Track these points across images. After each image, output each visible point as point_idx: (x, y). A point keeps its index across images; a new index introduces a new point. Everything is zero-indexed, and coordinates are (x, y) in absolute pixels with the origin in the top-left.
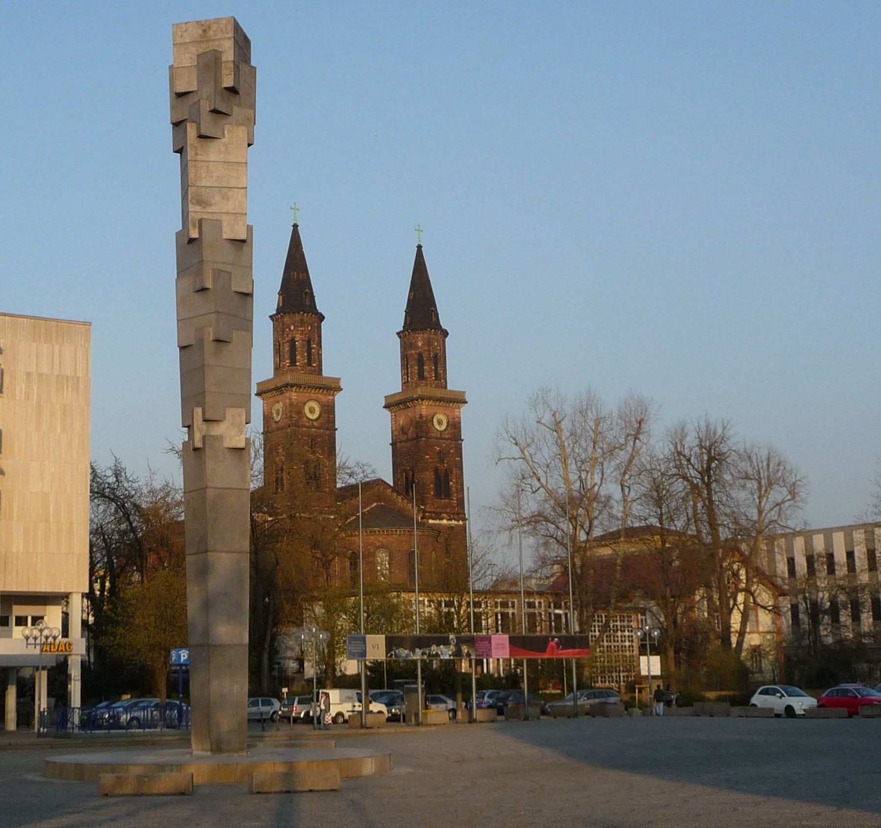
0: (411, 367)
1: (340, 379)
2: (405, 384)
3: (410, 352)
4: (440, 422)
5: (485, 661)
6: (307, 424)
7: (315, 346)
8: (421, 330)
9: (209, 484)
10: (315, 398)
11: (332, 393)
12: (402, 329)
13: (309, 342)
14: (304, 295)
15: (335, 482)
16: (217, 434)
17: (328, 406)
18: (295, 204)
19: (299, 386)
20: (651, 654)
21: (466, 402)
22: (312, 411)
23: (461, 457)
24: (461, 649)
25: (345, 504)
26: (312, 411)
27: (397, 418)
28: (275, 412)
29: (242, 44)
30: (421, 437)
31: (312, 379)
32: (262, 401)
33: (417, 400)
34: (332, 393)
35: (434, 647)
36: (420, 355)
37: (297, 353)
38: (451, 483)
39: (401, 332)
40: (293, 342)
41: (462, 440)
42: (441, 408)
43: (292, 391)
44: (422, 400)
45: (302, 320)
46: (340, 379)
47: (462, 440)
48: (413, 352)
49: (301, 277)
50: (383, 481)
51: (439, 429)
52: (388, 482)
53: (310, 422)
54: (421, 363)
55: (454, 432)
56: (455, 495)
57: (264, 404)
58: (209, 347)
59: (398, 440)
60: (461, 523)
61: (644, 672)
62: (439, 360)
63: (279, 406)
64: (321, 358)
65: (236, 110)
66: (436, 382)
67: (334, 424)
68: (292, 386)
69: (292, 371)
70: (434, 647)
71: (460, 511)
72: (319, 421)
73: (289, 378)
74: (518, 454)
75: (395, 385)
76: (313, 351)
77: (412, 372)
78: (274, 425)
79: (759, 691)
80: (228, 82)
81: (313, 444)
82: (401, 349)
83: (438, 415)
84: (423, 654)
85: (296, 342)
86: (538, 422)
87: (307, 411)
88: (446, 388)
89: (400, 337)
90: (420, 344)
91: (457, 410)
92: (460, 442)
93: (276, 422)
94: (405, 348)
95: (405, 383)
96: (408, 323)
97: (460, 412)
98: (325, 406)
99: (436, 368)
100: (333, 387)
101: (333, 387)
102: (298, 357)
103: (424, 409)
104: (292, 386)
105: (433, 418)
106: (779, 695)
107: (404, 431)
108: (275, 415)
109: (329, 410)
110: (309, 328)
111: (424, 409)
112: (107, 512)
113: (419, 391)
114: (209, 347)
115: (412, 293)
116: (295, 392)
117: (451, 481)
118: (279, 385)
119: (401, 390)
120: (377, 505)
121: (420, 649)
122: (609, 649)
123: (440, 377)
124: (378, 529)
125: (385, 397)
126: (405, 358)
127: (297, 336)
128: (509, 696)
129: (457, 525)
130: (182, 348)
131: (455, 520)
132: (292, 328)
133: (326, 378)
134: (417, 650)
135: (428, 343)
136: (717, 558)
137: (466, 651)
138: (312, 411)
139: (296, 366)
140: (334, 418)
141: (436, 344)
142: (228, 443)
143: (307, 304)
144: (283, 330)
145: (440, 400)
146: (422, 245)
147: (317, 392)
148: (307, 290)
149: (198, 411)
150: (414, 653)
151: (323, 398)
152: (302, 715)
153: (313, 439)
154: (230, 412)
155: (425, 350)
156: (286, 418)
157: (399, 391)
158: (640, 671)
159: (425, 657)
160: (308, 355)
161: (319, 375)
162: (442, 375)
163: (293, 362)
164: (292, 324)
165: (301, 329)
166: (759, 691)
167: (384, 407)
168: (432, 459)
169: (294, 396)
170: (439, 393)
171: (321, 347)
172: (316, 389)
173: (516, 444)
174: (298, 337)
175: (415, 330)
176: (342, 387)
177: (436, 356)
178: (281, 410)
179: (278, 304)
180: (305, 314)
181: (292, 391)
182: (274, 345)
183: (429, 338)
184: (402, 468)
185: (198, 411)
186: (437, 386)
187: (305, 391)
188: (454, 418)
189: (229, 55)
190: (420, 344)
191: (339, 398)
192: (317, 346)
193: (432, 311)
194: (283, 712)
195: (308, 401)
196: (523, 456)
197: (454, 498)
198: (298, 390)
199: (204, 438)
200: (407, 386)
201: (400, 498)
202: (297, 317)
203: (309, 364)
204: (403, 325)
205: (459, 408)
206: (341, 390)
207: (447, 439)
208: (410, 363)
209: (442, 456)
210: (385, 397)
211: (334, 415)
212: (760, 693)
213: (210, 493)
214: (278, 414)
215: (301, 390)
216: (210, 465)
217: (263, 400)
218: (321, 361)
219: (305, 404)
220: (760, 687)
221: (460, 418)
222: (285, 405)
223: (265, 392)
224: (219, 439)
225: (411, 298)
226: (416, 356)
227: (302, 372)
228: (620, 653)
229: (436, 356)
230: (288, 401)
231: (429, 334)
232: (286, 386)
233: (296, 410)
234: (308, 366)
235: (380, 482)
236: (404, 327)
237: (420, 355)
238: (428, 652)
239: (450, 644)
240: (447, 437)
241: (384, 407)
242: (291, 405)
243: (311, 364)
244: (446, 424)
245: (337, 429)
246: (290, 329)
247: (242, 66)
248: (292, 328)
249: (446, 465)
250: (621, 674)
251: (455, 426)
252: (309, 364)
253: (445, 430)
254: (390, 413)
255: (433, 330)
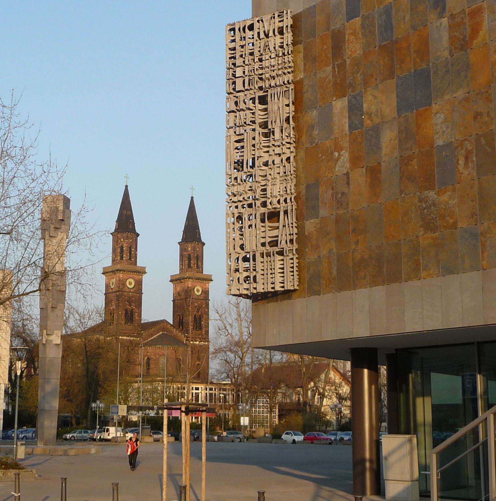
0: (185, 261)
1: (146, 267)
2: (181, 269)
3: (184, 253)
4: (198, 291)
5: (200, 418)
6: (127, 290)
7: (133, 250)
8: (190, 242)
9: (47, 356)
10: (132, 277)
11: (141, 274)
12: (181, 241)
13: (130, 248)
14: (129, 223)
15: (141, 321)
16: (51, 339)
17: (139, 281)
18: (127, 174)
19: (124, 271)
20: (245, 416)
21: (212, 281)
22: (130, 284)
23: (208, 309)
24: (159, 412)
25: (145, 332)
26: (130, 283)
27: (176, 287)
28: (111, 283)
29: (67, 201)
30: (187, 298)
31: (131, 267)
32: (105, 277)
33: (186, 279)
34: (141, 274)
35: (147, 411)
36: (189, 255)
37: (124, 253)
38: (202, 323)
39: (180, 242)
40: (122, 248)
41: (209, 300)
42: (199, 283)
43: (120, 273)
44: (189, 279)
45: (127, 236)
46: (146, 267)
47: (209, 300)
48: (186, 253)
49: (128, 214)
50: (166, 321)
51: (197, 294)
52: (170, 322)
53: (129, 289)
54: (189, 259)
55: (205, 296)
56: (204, 329)
57: (106, 278)
58: (49, 309)
59: (176, 299)
60: (206, 343)
61: (242, 424)
62: (199, 258)
63: (114, 280)
64: (137, 256)
65: (63, 226)
66: (197, 269)
67: (142, 290)
68: (120, 271)
69: (121, 263)
70: (147, 411)
71: (207, 337)
72: (134, 289)
73: (118, 267)
74: (218, 318)
75: (176, 271)
76: (132, 252)
77: (185, 264)
78: (110, 290)
79: (285, 433)
80: (60, 218)
81: (130, 302)
82: (180, 251)
83: (197, 287)
84: (142, 413)
85: (123, 247)
86: (229, 302)
87: (128, 284)
88: (203, 273)
89: (180, 245)
90: (189, 249)
91: (208, 284)
92: (208, 301)
93: (112, 289)
94: (182, 251)
95: (181, 269)
96: (184, 237)
97: (209, 285)
98: (137, 281)
99: (197, 263)
100: (142, 271)
101: (142, 271)
102: (124, 256)
103: (190, 283)
104: (120, 271)
105: (194, 288)
106: (291, 435)
107: (179, 294)
108: (111, 285)
109: (139, 283)
110: (131, 241)
111: (190, 283)
112: (17, 343)
113: (187, 274)
114: (49, 309)
115: (187, 222)
116: (122, 273)
117: (202, 321)
118: (114, 269)
119: (179, 273)
120: (163, 333)
121: (141, 411)
122: (259, 412)
123: (199, 267)
124: (161, 346)
125: (171, 276)
126: (181, 256)
127: (125, 244)
128: (196, 432)
129: (204, 344)
130: (41, 309)
131: (204, 342)
132: (122, 240)
133: (138, 267)
134: (140, 412)
135: (194, 249)
136: (302, 372)
137: (161, 413)
138: (130, 284)
139: (123, 260)
140: (142, 287)
141: (198, 250)
142: (54, 342)
143: (131, 228)
144: (117, 241)
145: (199, 279)
146: (194, 197)
147: (133, 273)
148: (131, 221)
149: (45, 331)
150: (139, 413)
151: (137, 277)
152: (98, 438)
153: (130, 298)
154: (56, 332)
155: (192, 253)
156: (117, 287)
157: (177, 273)
158: (240, 423)
159: (143, 415)
160: (129, 254)
161: (135, 265)
162: (200, 266)
163: (122, 258)
164: (122, 238)
165: (127, 241)
166: (285, 433)
167: (170, 281)
168: (193, 309)
169: (121, 276)
170: (198, 275)
171: (137, 250)
172: (133, 272)
173: (218, 313)
174: (125, 245)
175: (187, 242)
176: (146, 272)
177: (198, 255)
178: (114, 283)
179: (116, 227)
180: (129, 233)
181: (120, 273)
182: (113, 248)
183: (194, 246)
184: (178, 313)
185: (45, 331)
186: (197, 272)
187: (127, 273)
188: (206, 289)
189: (61, 208)
190: (189, 249)
191: (145, 278)
192: (135, 250)
193: (197, 232)
194: (90, 436)
195: (129, 278)
196: (220, 319)
197: (204, 330)
198: (123, 272)
199: (46, 340)
200: (182, 271)
201: (175, 329)
202: (125, 235)
203: (130, 259)
204: (181, 239)
205: (208, 283)
206: (146, 273)
207: (202, 300)
208: (184, 259)
209: (199, 308)
210: (171, 276)
211: (142, 286)
212: (285, 434)
213: (48, 359)
214: (113, 284)
215: (125, 273)
216: (48, 349)
217: (106, 276)
218: (137, 258)
219: (127, 280)
220: (285, 431)
221: (209, 288)
222: (116, 280)
223: (107, 273)
224: (52, 341)
225: (187, 224)
226: (187, 256)
227: (126, 263)
228: (261, 414)
229: (198, 255)
230: (118, 278)
231: (195, 244)
232: (117, 270)
233: (122, 283)
234: (130, 260)
235: (164, 321)
236: (182, 240)
237: (189, 255)
238: (145, 413)
239: (154, 410)
240: (201, 298)
241: (170, 281)
242: (120, 280)
243: (131, 259)
244: (201, 292)
245: (143, 293)
246: (121, 240)
247: (67, 210)
248: (122, 240)
249: (200, 313)
250: (257, 425)
251: (206, 293)
252: (130, 259)
253: (200, 295)
254: (173, 284)
255: (196, 243)
